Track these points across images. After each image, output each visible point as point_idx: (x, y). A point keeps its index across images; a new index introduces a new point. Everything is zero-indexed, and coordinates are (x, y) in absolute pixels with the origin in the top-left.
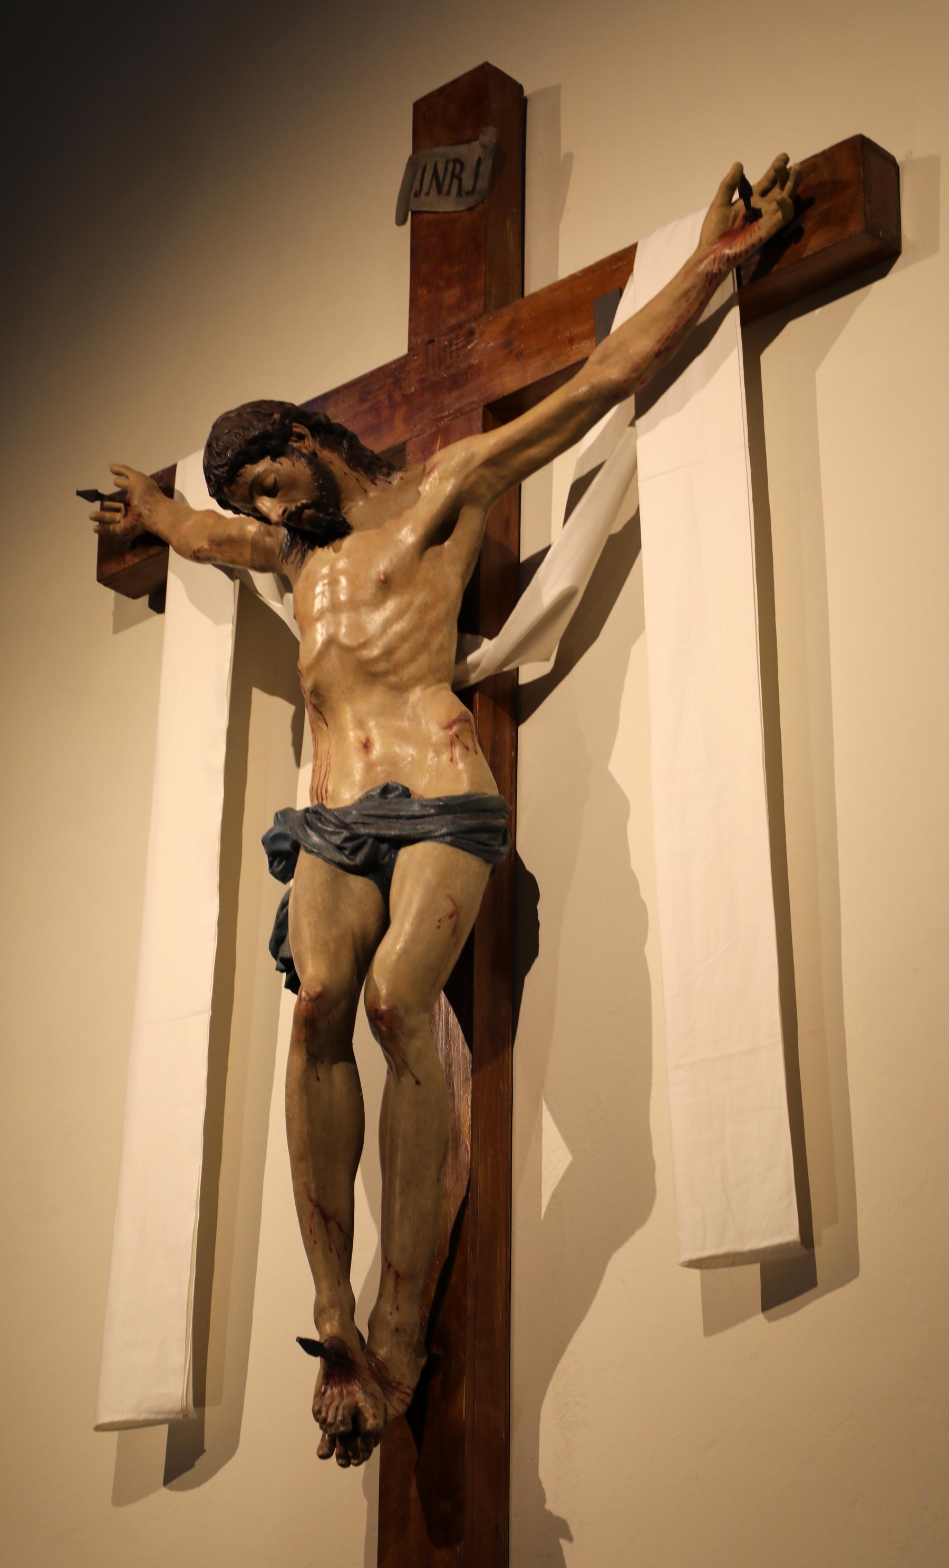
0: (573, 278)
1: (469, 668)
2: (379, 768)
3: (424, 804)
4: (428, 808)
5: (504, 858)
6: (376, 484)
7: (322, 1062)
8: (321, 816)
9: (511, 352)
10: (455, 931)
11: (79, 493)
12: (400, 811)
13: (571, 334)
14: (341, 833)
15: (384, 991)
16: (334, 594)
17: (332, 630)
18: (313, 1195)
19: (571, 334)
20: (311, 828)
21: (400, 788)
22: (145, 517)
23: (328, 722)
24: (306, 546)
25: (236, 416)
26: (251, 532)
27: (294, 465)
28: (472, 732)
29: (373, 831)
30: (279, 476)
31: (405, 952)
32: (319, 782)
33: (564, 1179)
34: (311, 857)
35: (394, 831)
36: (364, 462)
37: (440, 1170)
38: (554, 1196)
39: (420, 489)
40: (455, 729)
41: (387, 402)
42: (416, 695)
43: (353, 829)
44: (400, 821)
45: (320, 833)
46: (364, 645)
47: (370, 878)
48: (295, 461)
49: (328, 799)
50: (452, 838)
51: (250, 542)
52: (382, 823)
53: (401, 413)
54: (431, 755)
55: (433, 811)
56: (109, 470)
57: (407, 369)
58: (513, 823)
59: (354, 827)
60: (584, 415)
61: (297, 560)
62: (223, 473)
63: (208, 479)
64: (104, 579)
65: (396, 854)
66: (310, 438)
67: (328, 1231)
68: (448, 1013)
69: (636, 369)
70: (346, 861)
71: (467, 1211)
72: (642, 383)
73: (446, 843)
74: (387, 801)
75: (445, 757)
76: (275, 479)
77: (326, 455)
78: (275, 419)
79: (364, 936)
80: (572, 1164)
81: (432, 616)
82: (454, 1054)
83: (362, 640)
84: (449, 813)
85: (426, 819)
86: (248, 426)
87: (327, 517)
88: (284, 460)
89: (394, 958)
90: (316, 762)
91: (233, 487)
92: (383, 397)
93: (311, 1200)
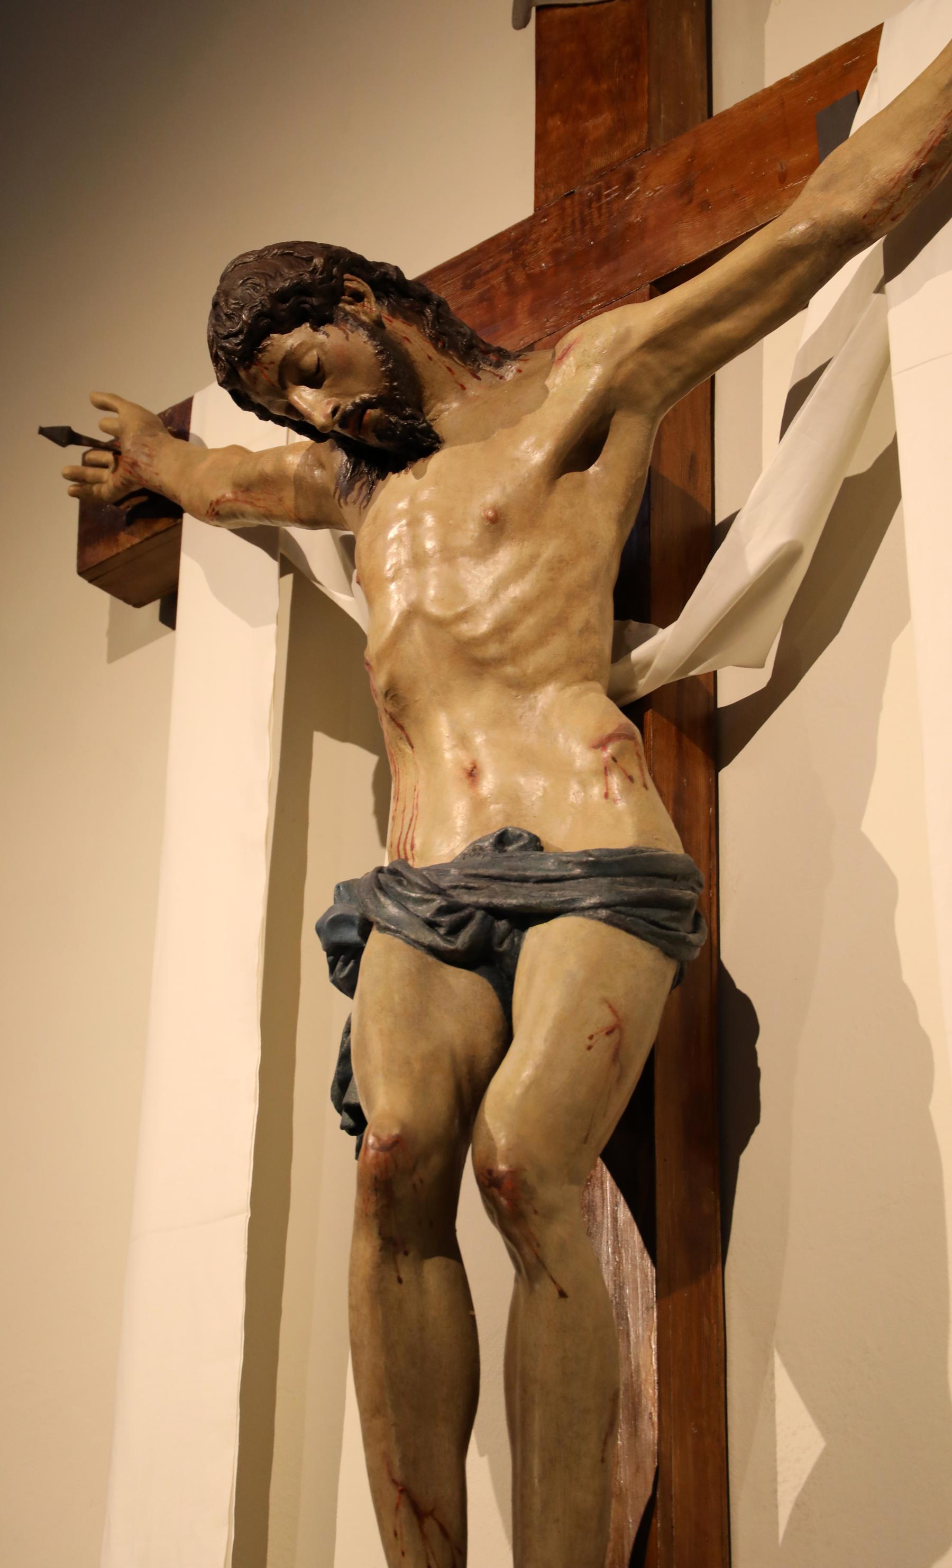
0: (784, 83)
1: (636, 669)
2: (492, 807)
3: (564, 860)
4: (570, 866)
5: (697, 953)
6: (479, 378)
7: (406, 1253)
8: (402, 878)
9: (691, 201)
10: (616, 1056)
11: (43, 431)
12: (525, 869)
13: (782, 168)
14: (433, 900)
15: (501, 1140)
16: (415, 541)
17: (413, 596)
18: (398, 1474)
19: (782, 168)
20: (386, 894)
21: (525, 835)
22: (143, 466)
23: (413, 742)
24: (374, 475)
25: (256, 260)
26: (293, 464)
27: (347, 338)
28: (638, 754)
29: (483, 900)
30: (325, 353)
31: (535, 1082)
32: (401, 834)
33: (812, 1478)
34: (387, 937)
35: (516, 898)
36: (460, 343)
37: (605, 1443)
38: (798, 1505)
39: (548, 383)
40: (610, 750)
41: (504, 288)
42: (547, 695)
43: (452, 896)
44: (526, 885)
45: (400, 901)
46: (463, 617)
47: (481, 974)
48: (349, 333)
49: (415, 857)
50: (608, 912)
51: (292, 479)
52: (496, 886)
53: (523, 305)
54: (575, 787)
55: (578, 871)
56: (99, 430)
57: (533, 237)
58: (714, 916)
59: (454, 893)
60: (801, 269)
61: (362, 497)
62: (238, 345)
63: (215, 358)
64: (89, 571)
65: (521, 938)
66: (373, 299)
67: (424, 1537)
68: (617, 1204)
69: (881, 197)
70: (442, 944)
71: (654, 1521)
72: (893, 219)
73: (600, 919)
74: (505, 855)
75: (596, 791)
76: (319, 359)
77: (397, 327)
78: (315, 265)
79: (471, 1062)
80: (826, 1453)
81: (570, 577)
82: (627, 1267)
83: (461, 609)
84: (605, 875)
85: (567, 883)
86: (273, 275)
87: (402, 422)
88: (329, 328)
89: (518, 1091)
90: (396, 805)
91: (254, 370)
92: (497, 280)
93: (394, 1482)
